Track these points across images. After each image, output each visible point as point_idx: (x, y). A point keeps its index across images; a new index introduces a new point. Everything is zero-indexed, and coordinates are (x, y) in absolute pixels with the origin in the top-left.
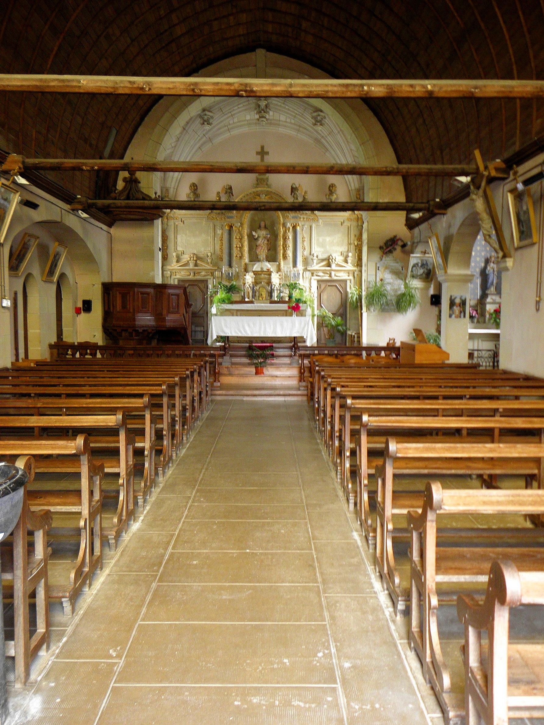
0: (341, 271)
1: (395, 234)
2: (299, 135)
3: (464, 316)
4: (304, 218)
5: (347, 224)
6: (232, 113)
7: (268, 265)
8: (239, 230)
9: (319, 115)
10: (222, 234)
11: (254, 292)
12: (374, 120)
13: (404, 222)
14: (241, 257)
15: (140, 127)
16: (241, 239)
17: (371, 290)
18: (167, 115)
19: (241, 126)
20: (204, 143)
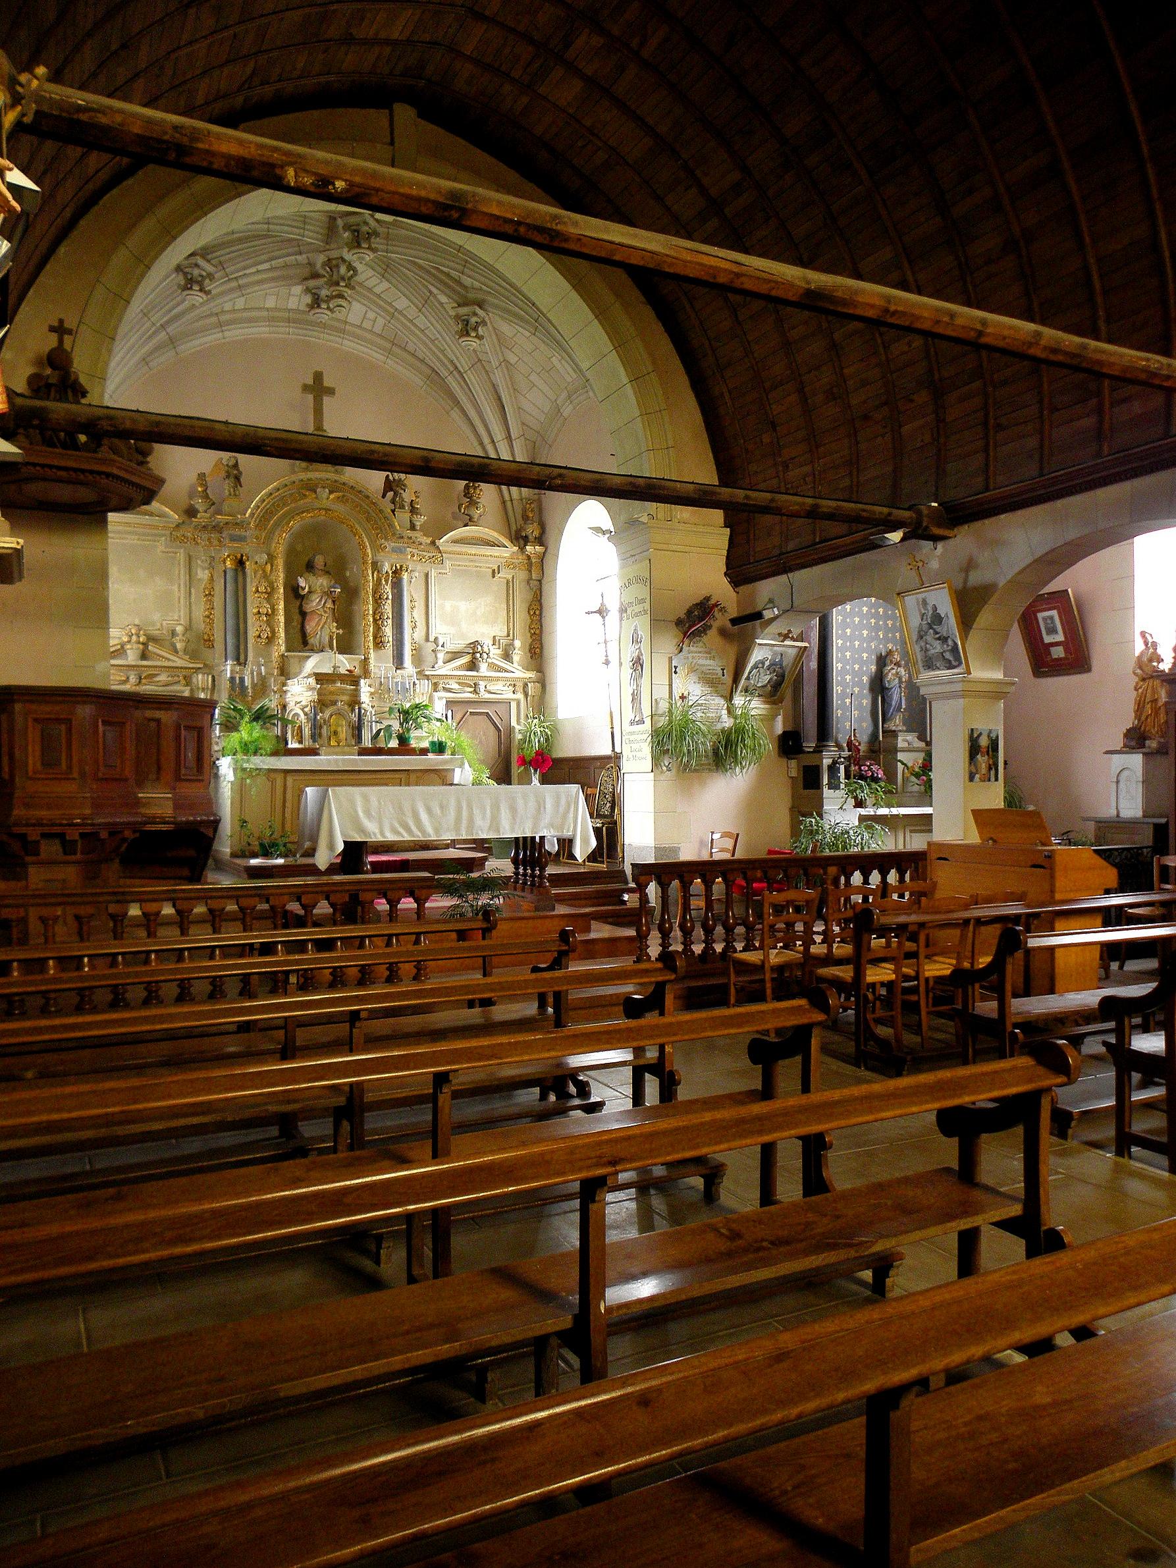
0: (498, 679)
1: (705, 593)
2: (389, 361)
3: (997, 779)
4: (413, 556)
5: (506, 574)
6: (241, 282)
7: (345, 663)
8: (264, 571)
9: (475, 314)
10: (212, 579)
11: (316, 728)
12: (658, 327)
13: (724, 569)
14: (271, 640)
15: (65, 243)
16: (270, 594)
17: (662, 721)
18: (148, 225)
19: (250, 320)
20: (157, 348)
